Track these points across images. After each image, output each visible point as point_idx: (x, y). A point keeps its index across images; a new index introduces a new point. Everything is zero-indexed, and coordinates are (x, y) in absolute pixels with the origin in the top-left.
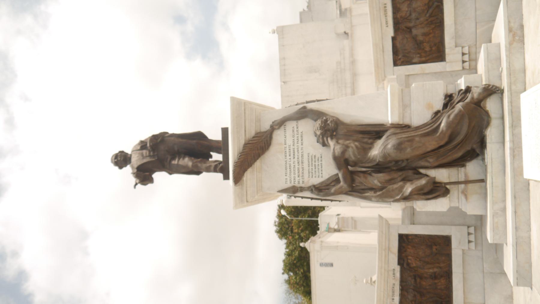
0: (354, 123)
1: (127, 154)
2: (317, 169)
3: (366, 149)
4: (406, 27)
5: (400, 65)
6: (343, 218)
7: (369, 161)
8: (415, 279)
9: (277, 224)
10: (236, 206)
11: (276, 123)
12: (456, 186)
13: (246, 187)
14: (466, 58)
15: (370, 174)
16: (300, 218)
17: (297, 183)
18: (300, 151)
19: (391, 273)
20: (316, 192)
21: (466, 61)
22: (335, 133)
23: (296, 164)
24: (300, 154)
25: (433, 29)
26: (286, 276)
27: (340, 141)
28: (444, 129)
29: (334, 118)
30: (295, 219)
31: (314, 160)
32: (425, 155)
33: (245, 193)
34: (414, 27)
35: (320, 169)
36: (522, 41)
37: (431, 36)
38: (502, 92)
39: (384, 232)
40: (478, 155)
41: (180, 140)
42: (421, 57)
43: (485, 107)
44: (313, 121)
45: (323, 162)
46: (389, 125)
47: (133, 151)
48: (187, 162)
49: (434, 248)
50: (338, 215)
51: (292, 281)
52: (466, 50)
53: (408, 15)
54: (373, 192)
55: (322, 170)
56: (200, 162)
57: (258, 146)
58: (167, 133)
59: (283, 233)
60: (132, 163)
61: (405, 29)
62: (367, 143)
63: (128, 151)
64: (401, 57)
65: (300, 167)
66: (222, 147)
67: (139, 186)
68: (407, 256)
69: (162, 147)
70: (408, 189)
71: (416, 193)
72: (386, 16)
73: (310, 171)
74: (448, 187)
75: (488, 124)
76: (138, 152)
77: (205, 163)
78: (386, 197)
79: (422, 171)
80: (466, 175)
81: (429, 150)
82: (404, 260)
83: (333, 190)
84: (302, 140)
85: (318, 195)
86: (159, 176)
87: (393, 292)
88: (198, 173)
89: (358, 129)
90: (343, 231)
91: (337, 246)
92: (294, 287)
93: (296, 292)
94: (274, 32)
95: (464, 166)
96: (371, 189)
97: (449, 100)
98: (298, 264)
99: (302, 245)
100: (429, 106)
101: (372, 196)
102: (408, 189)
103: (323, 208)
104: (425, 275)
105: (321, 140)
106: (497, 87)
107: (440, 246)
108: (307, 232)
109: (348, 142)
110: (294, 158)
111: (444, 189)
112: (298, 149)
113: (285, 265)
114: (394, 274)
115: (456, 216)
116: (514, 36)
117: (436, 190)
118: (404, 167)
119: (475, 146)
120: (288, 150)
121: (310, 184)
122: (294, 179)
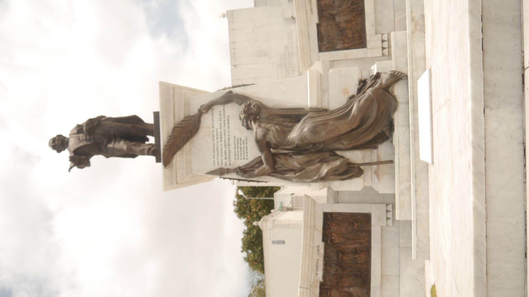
0: (276, 107)
1: (66, 138)
2: (242, 151)
3: (285, 132)
4: (330, 14)
5: (325, 51)
6: (297, 197)
7: (288, 145)
8: (338, 254)
9: (236, 203)
10: (166, 188)
11: (204, 107)
12: (370, 166)
13: (176, 170)
14: (386, 45)
15: (291, 156)
16: (257, 198)
17: (224, 165)
18: (227, 134)
19: (316, 249)
20: (241, 174)
21: (385, 48)
22: (258, 117)
23: (223, 147)
24: (227, 137)
25: (355, 17)
26: (245, 254)
27: (262, 125)
28: (356, 113)
29: (258, 103)
30: (253, 198)
31: (239, 143)
32: (339, 138)
33: (175, 175)
34: (337, 14)
35: (246, 152)
36: (423, 30)
37: (353, 23)
38: (407, 76)
39: (310, 211)
40: (388, 138)
41: (116, 124)
42: (344, 43)
43: (393, 92)
44: (239, 106)
45: (248, 145)
46: (308, 109)
47: (70, 135)
48: (122, 145)
49: (356, 224)
50: (292, 194)
51: (251, 258)
52: (385, 37)
53: (331, 2)
54: (293, 173)
55: (247, 153)
56: (135, 145)
57: (187, 130)
58: (104, 117)
59: (241, 212)
60: (69, 147)
61: (329, 16)
62: (287, 126)
63: (66, 135)
64: (326, 43)
65: (227, 149)
66: (154, 130)
67: (75, 168)
68: (331, 233)
69: (98, 131)
70: (325, 170)
71: (332, 173)
72: (311, 4)
73: (237, 153)
74: (362, 167)
75: (395, 109)
76: (75, 135)
77: (139, 146)
78: (305, 178)
79: (339, 153)
80: (378, 156)
81: (342, 133)
82: (328, 237)
83: (256, 172)
84: (228, 124)
85: (243, 176)
86: (97, 160)
87: (317, 267)
88: (134, 156)
89: (279, 112)
90: (295, 209)
91: (289, 225)
92: (252, 264)
93: (255, 269)
94: (224, 16)
95: (376, 148)
96: (292, 170)
97: (363, 83)
98: (256, 242)
99: (255, 223)
100: (345, 91)
101: (293, 177)
102: (325, 170)
103: (278, 188)
104: (347, 251)
105: (245, 124)
106: (402, 74)
107: (361, 223)
108: (265, 211)
109: (269, 125)
110: (221, 141)
111: (357, 170)
112: (224, 132)
113: (244, 244)
114: (318, 250)
115: (369, 195)
116: (416, 25)
117: (351, 171)
118: (322, 149)
119: (384, 129)
120: (215, 134)
121: (236, 166)
122: (222, 161)
